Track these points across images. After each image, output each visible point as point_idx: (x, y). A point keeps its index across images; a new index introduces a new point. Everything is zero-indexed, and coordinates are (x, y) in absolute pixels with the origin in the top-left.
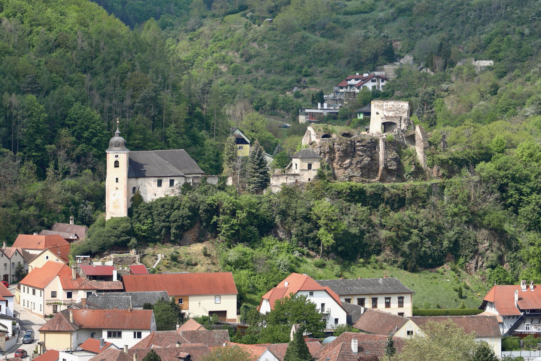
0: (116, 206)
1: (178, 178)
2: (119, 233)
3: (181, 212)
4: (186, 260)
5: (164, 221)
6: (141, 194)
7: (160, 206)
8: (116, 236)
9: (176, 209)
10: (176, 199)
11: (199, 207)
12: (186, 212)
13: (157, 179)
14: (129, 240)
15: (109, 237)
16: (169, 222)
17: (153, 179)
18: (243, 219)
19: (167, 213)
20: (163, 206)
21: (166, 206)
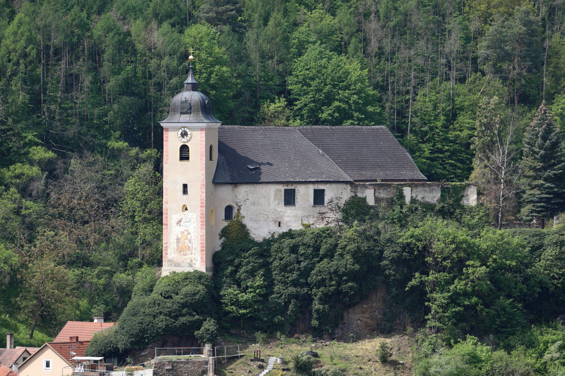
0: (181, 250)
1: (334, 186)
2: (175, 307)
3: (335, 262)
4: (332, 370)
5: (295, 283)
6: (245, 221)
7: (287, 250)
8: (169, 314)
9: (325, 256)
10: (326, 233)
11: (382, 252)
12: (347, 262)
13: (282, 188)
14: (198, 325)
15: (155, 317)
16: (307, 284)
17: (272, 189)
18: (479, 279)
19: (303, 264)
20: (294, 249)
21: (301, 250)
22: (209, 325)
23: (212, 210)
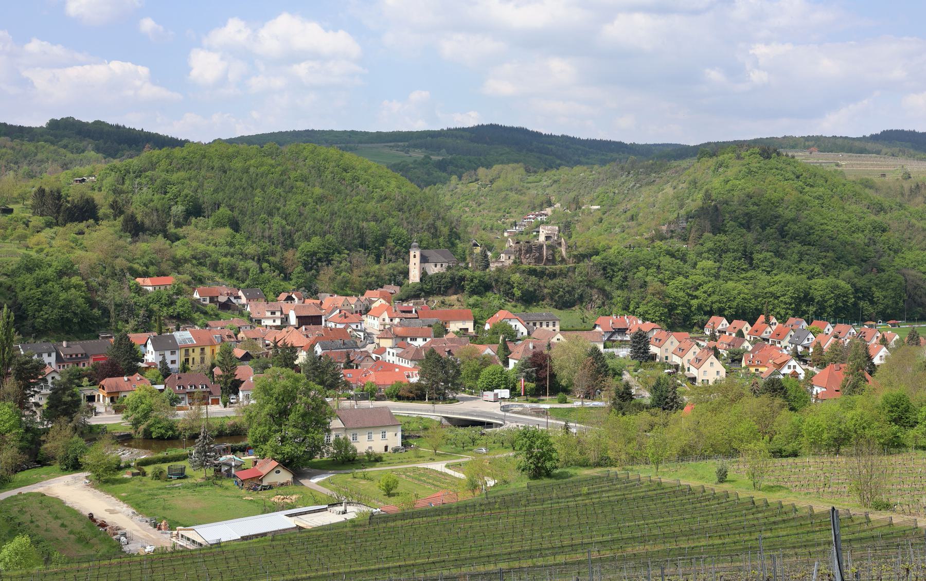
12: (448, 280)
22: (423, 294)
23: (10, 211)
